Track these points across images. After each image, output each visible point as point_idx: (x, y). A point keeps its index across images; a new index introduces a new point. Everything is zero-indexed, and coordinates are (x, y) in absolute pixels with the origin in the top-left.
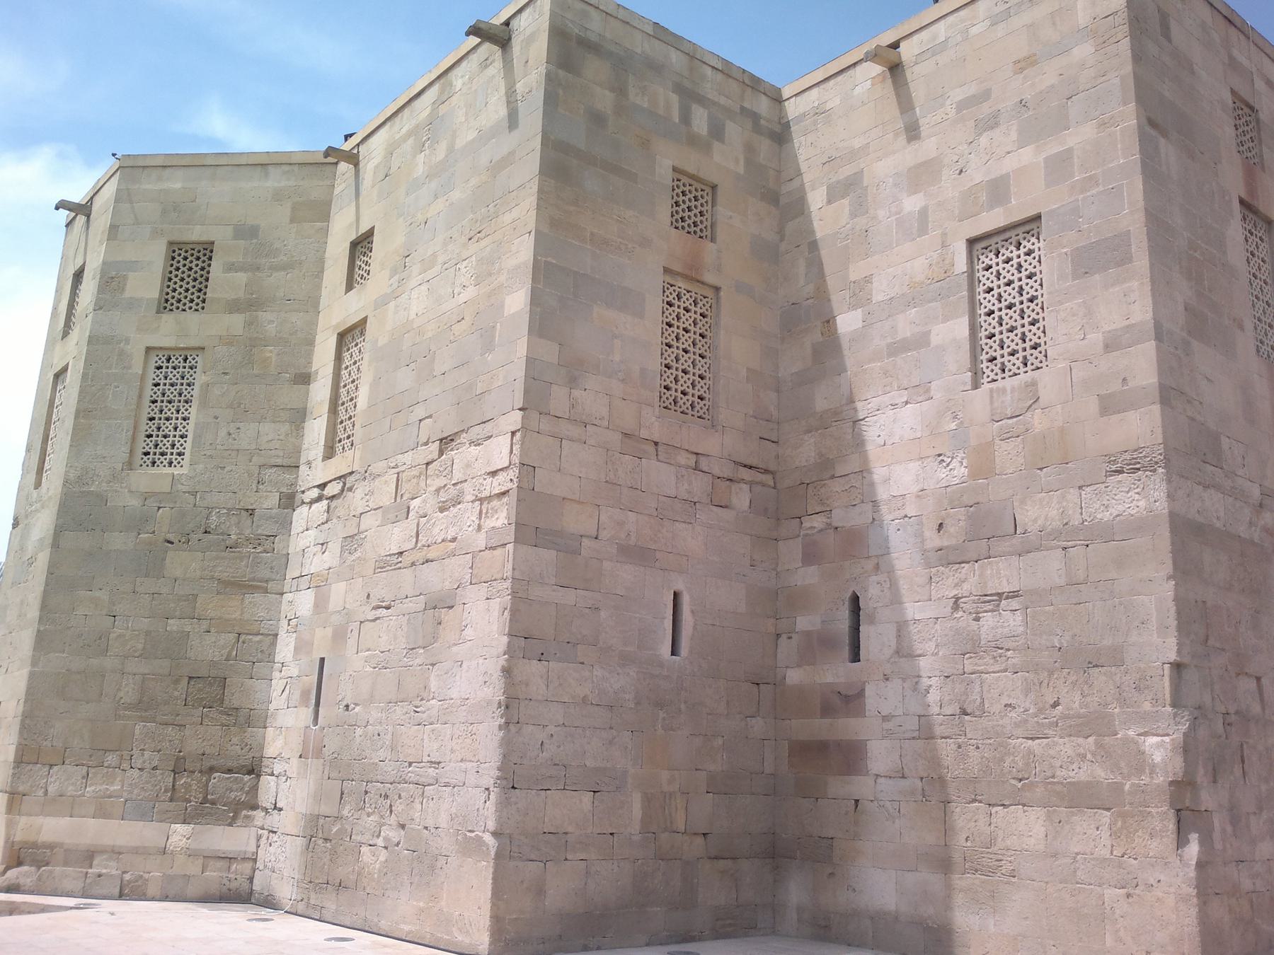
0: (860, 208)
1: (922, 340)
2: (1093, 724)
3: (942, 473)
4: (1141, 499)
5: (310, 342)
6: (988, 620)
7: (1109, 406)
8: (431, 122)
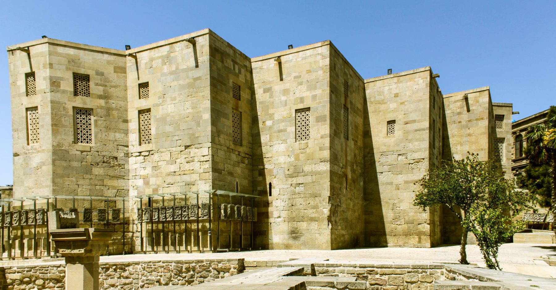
0: (271, 96)
1: (285, 130)
2: (315, 207)
3: (289, 159)
4: (326, 167)
6: (297, 188)
7: (321, 149)
8: (168, 56)
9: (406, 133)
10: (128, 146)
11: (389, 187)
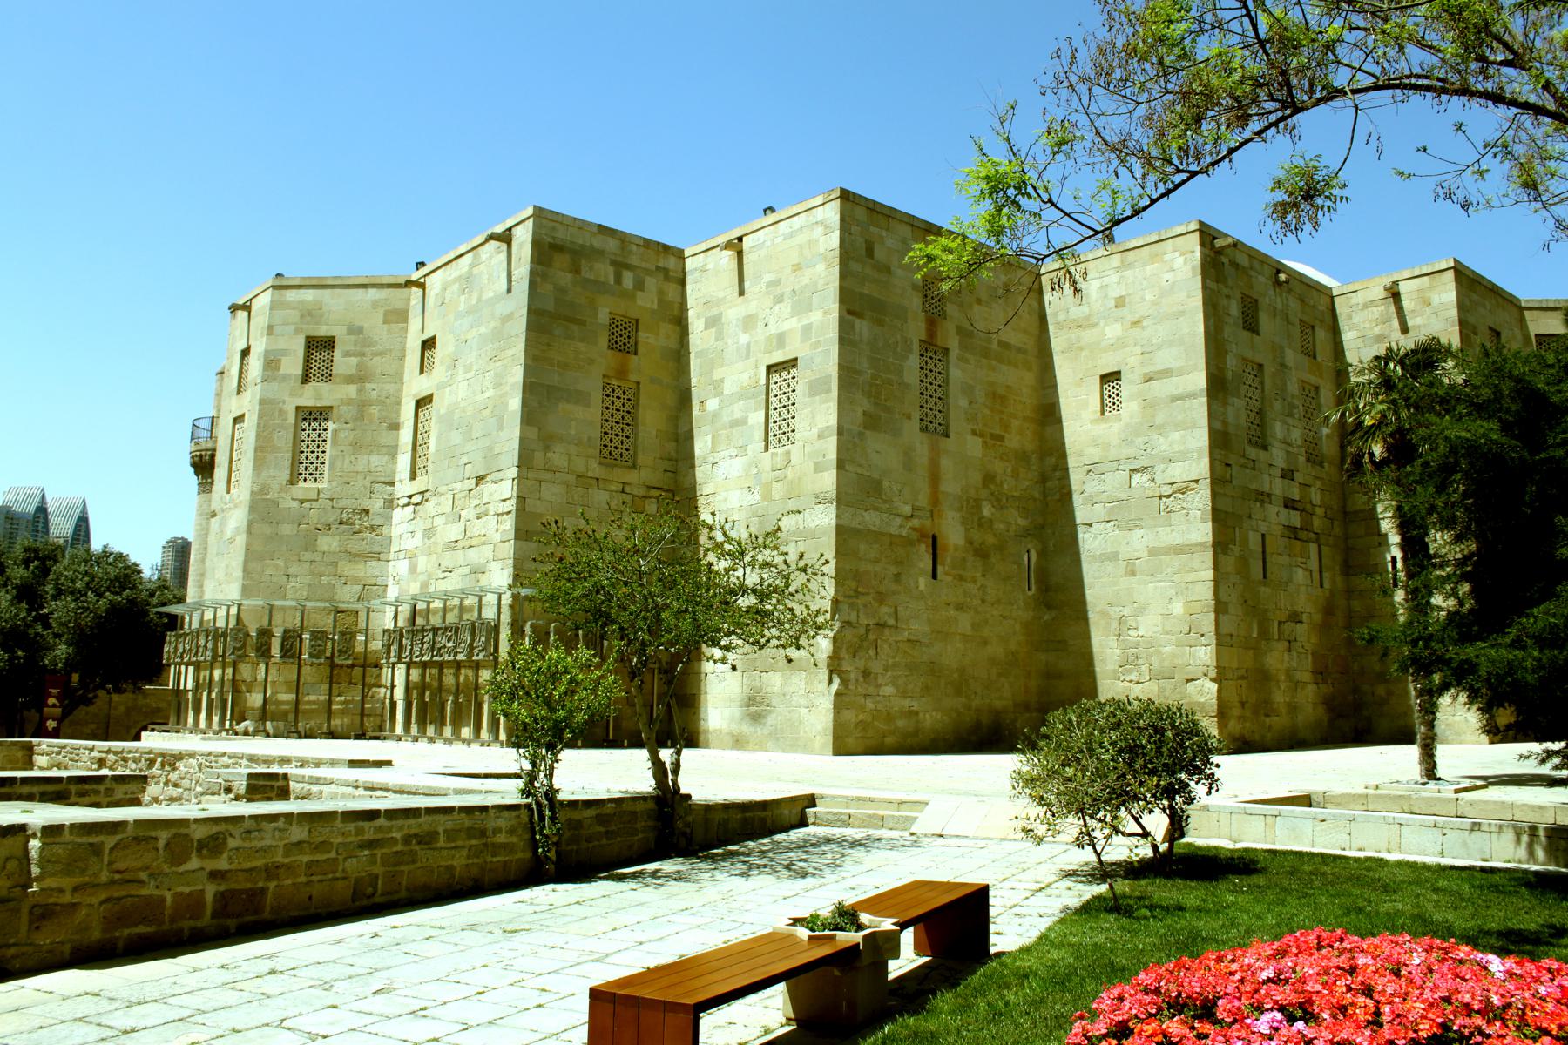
0: (720, 336)
1: (742, 422)
5: (399, 403)
7: (818, 468)
9: (1149, 405)
10: (392, 484)
11: (1110, 567)
